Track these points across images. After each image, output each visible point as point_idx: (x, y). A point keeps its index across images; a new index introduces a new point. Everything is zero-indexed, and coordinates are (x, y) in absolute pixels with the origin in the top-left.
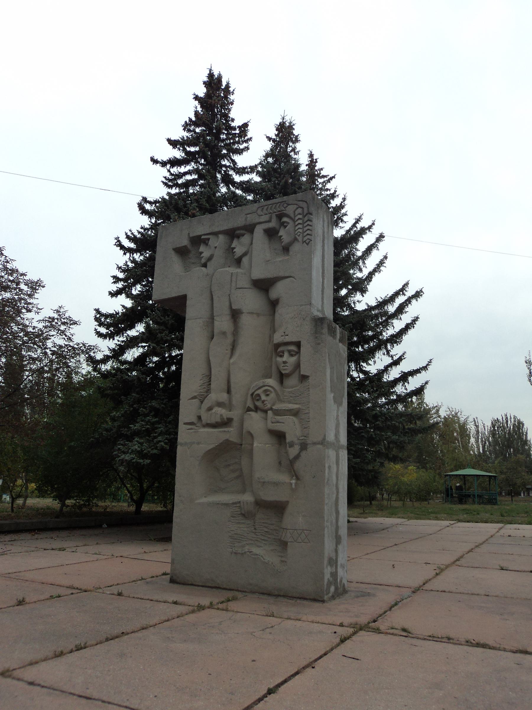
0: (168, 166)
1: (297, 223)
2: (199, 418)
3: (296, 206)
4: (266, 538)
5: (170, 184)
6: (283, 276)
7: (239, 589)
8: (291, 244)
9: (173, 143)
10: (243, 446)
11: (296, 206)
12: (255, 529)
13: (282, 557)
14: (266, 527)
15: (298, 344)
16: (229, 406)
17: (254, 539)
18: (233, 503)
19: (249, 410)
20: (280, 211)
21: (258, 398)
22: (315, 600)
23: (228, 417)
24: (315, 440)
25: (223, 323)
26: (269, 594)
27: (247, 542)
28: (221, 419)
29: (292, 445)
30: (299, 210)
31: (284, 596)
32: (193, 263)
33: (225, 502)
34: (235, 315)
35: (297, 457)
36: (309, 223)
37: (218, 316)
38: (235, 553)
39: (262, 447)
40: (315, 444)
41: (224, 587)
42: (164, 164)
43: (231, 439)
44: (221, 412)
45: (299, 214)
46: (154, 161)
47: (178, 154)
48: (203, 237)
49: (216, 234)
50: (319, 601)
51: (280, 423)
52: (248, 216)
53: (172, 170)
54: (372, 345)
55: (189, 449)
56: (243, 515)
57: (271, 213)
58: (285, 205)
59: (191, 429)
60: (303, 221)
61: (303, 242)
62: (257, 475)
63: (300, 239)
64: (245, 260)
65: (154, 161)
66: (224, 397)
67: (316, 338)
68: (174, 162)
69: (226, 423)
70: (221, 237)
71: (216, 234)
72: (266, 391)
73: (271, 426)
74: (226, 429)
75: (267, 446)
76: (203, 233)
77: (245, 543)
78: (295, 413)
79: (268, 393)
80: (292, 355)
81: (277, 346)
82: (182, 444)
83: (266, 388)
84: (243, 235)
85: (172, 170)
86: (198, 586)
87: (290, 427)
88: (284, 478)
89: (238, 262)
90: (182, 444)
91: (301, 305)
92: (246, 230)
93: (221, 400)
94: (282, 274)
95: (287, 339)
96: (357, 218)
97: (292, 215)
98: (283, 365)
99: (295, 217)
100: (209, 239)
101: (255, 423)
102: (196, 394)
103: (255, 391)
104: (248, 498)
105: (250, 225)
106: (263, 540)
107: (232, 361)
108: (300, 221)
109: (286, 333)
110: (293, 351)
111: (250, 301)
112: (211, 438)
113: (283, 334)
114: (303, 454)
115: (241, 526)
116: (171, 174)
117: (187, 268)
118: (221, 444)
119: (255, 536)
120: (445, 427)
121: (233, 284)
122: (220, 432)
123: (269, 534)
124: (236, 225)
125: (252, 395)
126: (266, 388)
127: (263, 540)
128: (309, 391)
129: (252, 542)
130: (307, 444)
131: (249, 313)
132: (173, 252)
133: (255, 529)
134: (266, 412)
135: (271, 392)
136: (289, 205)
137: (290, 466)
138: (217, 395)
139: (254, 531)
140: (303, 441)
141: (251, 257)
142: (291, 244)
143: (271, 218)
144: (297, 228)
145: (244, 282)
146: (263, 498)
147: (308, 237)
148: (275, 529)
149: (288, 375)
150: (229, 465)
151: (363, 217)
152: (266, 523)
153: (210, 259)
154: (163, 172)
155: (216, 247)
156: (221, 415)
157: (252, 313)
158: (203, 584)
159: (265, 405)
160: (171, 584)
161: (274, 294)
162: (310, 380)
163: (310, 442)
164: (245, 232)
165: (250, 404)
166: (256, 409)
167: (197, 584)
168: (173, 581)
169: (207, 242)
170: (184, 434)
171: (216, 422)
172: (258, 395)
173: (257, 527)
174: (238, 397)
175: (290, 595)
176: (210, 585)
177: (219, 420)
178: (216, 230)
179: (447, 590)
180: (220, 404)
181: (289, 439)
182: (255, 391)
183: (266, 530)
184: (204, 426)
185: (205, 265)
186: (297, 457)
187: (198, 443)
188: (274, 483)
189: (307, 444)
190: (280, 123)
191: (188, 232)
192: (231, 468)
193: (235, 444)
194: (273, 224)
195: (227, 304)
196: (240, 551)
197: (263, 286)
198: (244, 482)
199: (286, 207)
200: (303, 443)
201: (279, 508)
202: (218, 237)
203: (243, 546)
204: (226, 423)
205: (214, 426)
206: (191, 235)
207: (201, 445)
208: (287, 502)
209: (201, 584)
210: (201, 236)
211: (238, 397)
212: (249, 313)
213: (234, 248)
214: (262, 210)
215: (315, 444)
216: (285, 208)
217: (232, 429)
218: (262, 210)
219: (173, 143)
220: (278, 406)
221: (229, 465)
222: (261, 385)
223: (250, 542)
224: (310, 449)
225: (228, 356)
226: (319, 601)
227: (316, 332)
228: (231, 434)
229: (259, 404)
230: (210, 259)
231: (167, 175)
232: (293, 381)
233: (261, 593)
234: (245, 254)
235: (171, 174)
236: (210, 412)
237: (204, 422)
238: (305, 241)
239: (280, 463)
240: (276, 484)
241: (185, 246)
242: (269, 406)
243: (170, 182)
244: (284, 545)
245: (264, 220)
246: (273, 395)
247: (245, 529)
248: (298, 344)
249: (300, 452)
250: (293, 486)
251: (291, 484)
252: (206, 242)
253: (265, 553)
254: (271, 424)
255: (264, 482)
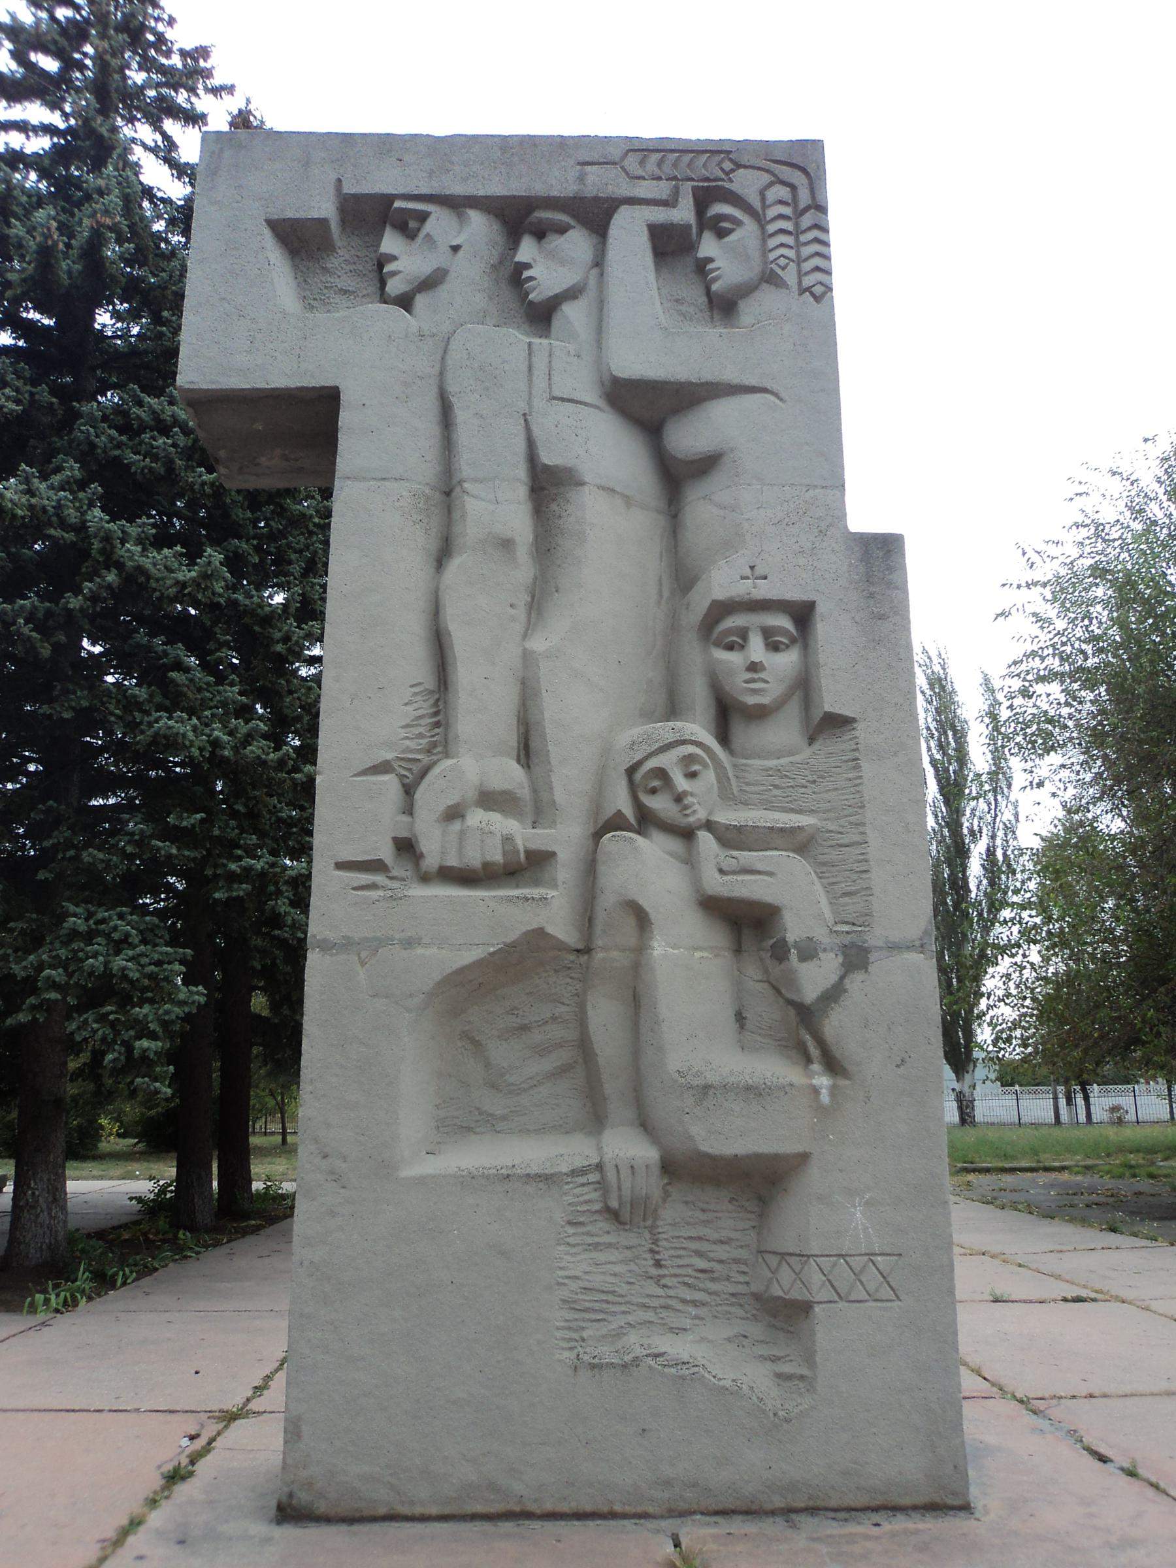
1: (771, 228)
2: (406, 847)
3: (766, 178)
4: (699, 1296)
6: (736, 381)
7: (618, 1508)
8: (746, 290)
10: (599, 955)
11: (766, 178)
12: (658, 1264)
13: (775, 1359)
14: (699, 1254)
15: (803, 614)
16: (540, 810)
17: (655, 1303)
18: (574, 1173)
19: (616, 823)
20: (707, 179)
21: (656, 783)
22: (933, 1508)
23: (533, 846)
24: (896, 936)
25: (497, 506)
26: (751, 1512)
27: (630, 1318)
28: (504, 854)
29: (809, 952)
30: (783, 192)
31: (813, 1510)
32: (345, 292)
33: (534, 1169)
34: (547, 485)
35: (833, 995)
36: (815, 233)
37: (476, 480)
38: (593, 1367)
39: (686, 964)
40: (894, 948)
41: (549, 1506)
43: (550, 930)
44: (493, 833)
45: (781, 202)
48: (398, 204)
49: (456, 204)
50: (953, 1508)
51: (759, 872)
52: (589, 168)
54: (111, 801)
55: (363, 963)
56: (614, 1215)
57: (675, 178)
58: (728, 166)
59: (373, 886)
60: (797, 225)
61: (803, 291)
62: (675, 1061)
63: (790, 276)
64: (574, 314)
66: (508, 774)
67: (871, 595)
69: (524, 868)
70: (476, 218)
71: (456, 204)
72: (689, 759)
73: (716, 884)
74: (536, 892)
75: (698, 954)
76: (401, 190)
77: (621, 1321)
78: (800, 843)
79: (696, 767)
80: (774, 647)
81: (722, 609)
82: (326, 946)
83: (691, 749)
84: (562, 230)
86: (424, 1518)
87: (796, 892)
88: (774, 1068)
89: (542, 316)
90: (326, 946)
91: (809, 487)
92: (575, 217)
93: (497, 783)
94: (731, 375)
95: (763, 590)
97: (756, 203)
98: (748, 676)
99: (765, 206)
100: (423, 217)
101: (647, 869)
102: (390, 756)
103: (646, 758)
104: (627, 1149)
105: (607, 199)
106: (694, 1303)
107: (538, 644)
108: (782, 224)
109: (759, 571)
110: (785, 632)
111: (604, 452)
112: (468, 926)
113: (748, 572)
114: (855, 982)
115: (601, 1257)
117: (311, 301)
118: (513, 945)
119: (660, 1292)
121: (540, 382)
122: (510, 900)
123: (713, 1280)
124: (539, 189)
125: (631, 771)
126: (691, 749)
127: (694, 1303)
128: (857, 767)
129: (650, 1316)
130: (867, 951)
131: (603, 488)
132: (267, 232)
133: (658, 1264)
134: (687, 834)
135: (705, 766)
136: (739, 166)
137: (804, 1030)
138: (479, 759)
139: (654, 1271)
140: (847, 940)
141: (601, 304)
142: (746, 290)
143: (676, 192)
144: (772, 243)
145: (580, 381)
146: (705, 1147)
147: (819, 276)
148: (736, 1261)
149: (760, 714)
150: (524, 1028)
152: (700, 1238)
153: (430, 283)
155: (456, 249)
156: (508, 839)
157: (610, 490)
158: (447, 1511)
159: (686, 807)
160: (290, 1532)
161: (689, 436)
162: (860, 730)
163: (880, 944)
164: (572, 222)
165: (621, 801)
166: (645, 821)
167: (418, 1510)
168: (289, 1512)
169: (412, 224)
170: (335, 909)
171: (486, 865)
172: (662, 774)
173: (664, 1255)
174: (570, 778)
175: (833, 1503)
176: (479, 1508)
177: (497, 857)
178: (458, 189)
179: (1047, 1396)
180: (490, 800)
181: (794, 929)
182: (646, 758)
183: (701, 1264)
184: (424, 879)
185: (405, 302)
186: (833, 995)
187: (409, 943)
188: (748, 1088)
189: (867, 951)
190: (240, 111)
191: (334, 176)
192: (537, 1037)
193: (561, 946)
194: (684, 213)
195: (520, 446)
196: (606, 1352)
197: (647, 407)
198: (590, 1091)
199: (732, 171)
200: (853, 945)
201: (760, 1183)
202: (461, 217)
203: (618, 1335)
204: (524, 868)
205: (465, 878)
206: (349, 188)
207: (420, 951)
208: (803, 1158)
209: (434, 1510)
210: (389, 199)
211: (570, 778)
212: (603, 488)
213: (528, 266)
214: (642, 163)
215: (894, 948)
216: (727, 174)
217: (551, 893)
218: (642, 163)
220: (726, 817)
221: (524, 1028)
222: (671, 737)
223: (642, 1315)
224: (879, 965)
225: (519, 627)
226: (953, 1508)
227: (869, 579)
228: (552, 909)
229: (659, 804)
230: (430, 283)
232: (783, 732)
233: (717, 1513)
234: (571, 294)
236: (456, 826)
237: (431, 862)
238: (808, 289)
239: (740, 1018)
240: (754, 1092)
241: (323, 222)
242: (702, 815)
244: (787, 1316)
245: (650, 196)
246: (709, 777)
247: (618, 1269)
248: (803, 614)
249: (842, 978)
250: (825, 1097)
251: (816, 1091)
252: (409, 225)
253: (712, 1351)
254: (717, 875)
255: (707, 1088)
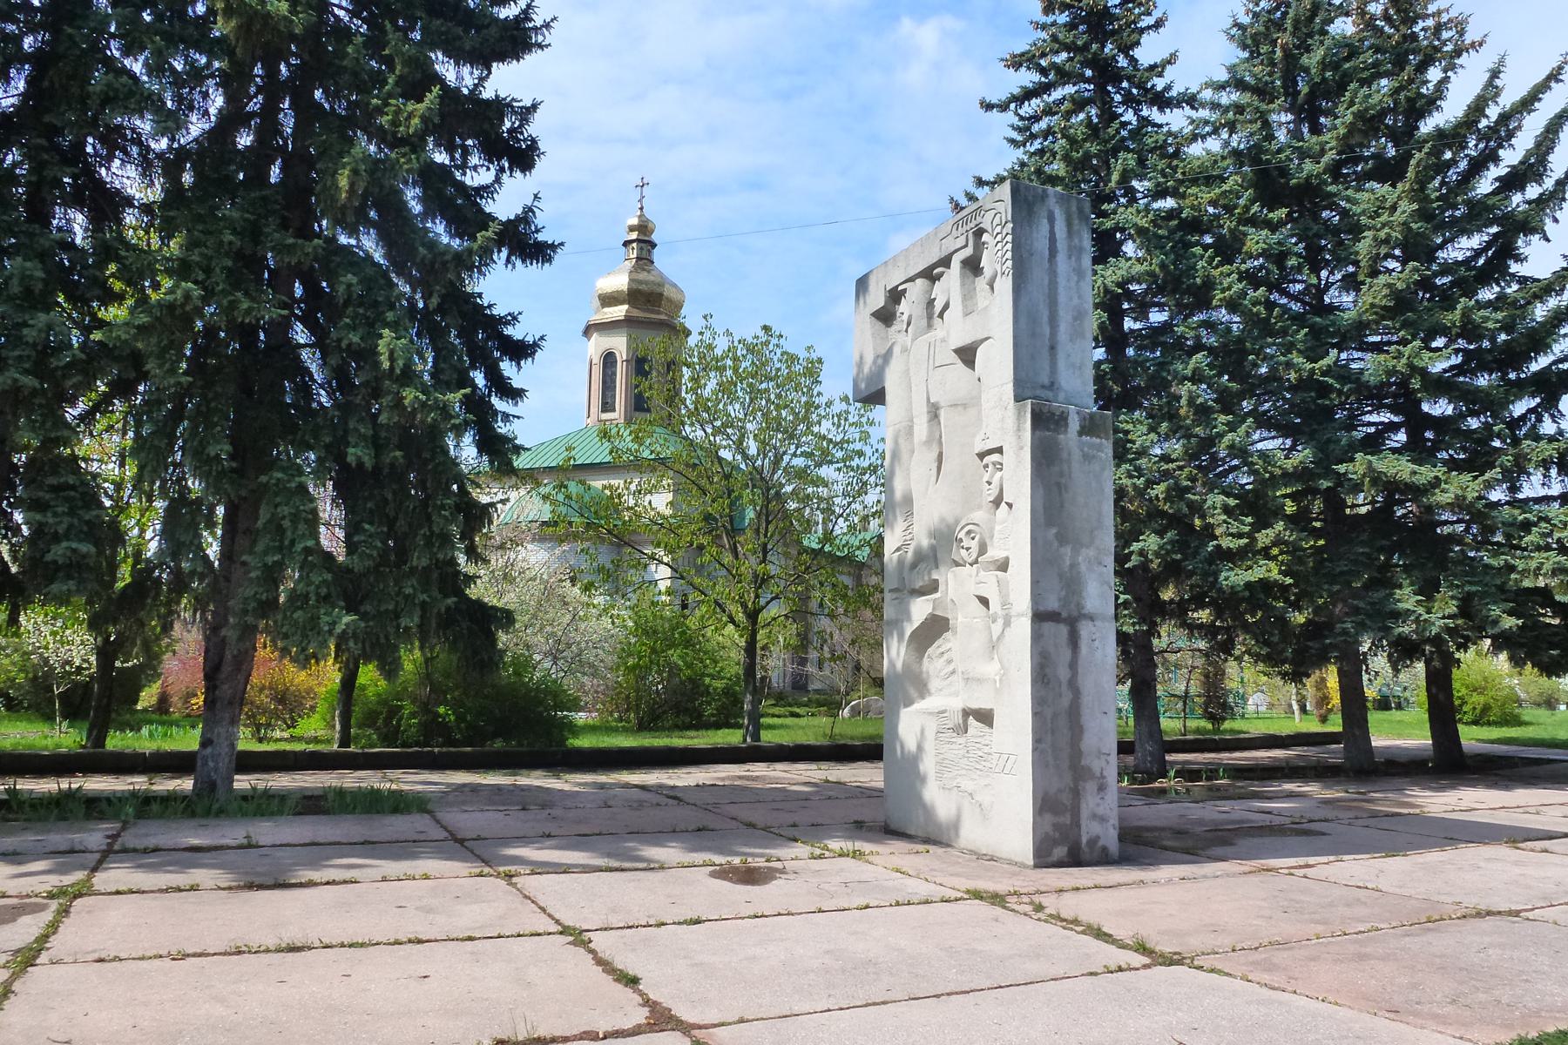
0: (1013, 106)
5: (1020, 138)
9: (1016, 62)
42: (1003, 107)
46: (988, 107)
47: (1028, 78)
53: (353, 242)
65: (988, 107)
68: (1028, 94)
72: (969, 532)
85: (1021, 112)
96: (1491, 66)
116: (1022, 118)
120: (177, 229)
151: (1508, 61)
154: (1010, 117)
219: (1016, 62)
231: (1016, 121)
235: (1022, 118)
243: (1025, 129)
